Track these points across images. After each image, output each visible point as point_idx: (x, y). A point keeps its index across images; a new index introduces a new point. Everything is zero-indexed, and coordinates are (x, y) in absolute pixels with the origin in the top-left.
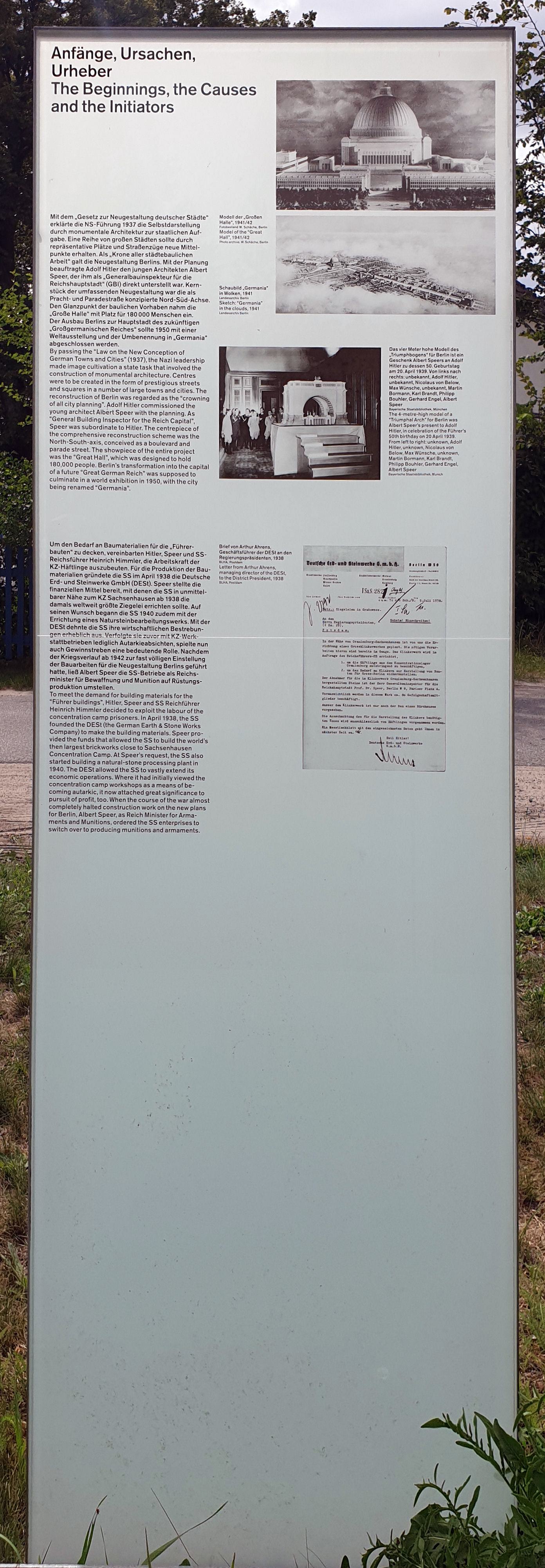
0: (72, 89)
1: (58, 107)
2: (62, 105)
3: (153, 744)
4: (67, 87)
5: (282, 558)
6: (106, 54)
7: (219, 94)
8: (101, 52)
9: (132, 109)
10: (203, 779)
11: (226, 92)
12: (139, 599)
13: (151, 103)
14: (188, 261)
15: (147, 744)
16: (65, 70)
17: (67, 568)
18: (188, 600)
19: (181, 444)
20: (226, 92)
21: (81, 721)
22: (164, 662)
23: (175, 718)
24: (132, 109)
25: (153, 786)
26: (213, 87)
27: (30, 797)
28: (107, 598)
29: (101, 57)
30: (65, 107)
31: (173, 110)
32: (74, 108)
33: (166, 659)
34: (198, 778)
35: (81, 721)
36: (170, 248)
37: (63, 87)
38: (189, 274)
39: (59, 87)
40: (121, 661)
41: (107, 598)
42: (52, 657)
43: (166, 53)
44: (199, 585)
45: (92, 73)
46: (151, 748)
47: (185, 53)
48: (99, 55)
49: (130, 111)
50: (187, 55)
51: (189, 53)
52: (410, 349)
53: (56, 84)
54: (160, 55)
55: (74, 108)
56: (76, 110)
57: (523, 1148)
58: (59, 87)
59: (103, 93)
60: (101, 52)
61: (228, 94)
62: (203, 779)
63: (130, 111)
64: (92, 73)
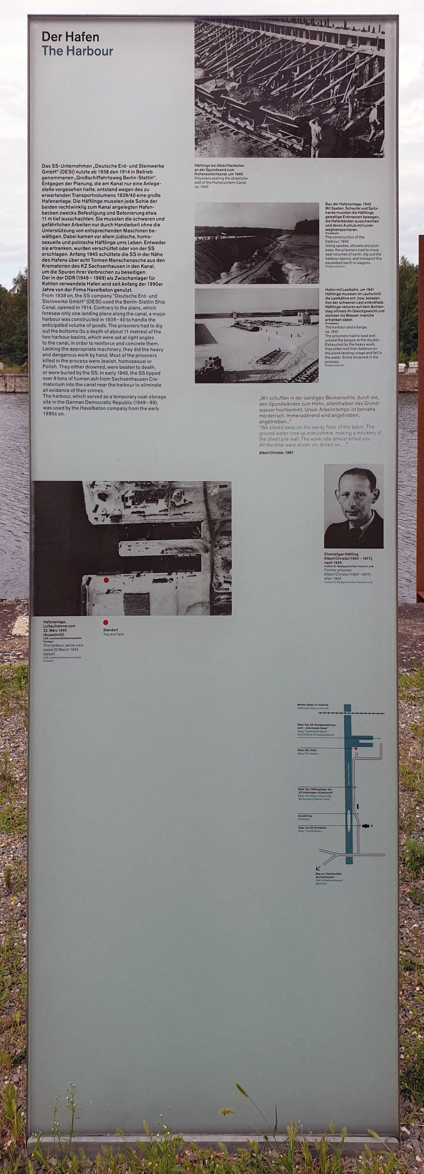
0: (58, 51)
10: (163, 166)
12: (113, 267)
14: (76, 183)
18: (154, 320)
21: (62, 400)
27: (27, 424)
28: (88, 266)
35: (62, 400)
37: (51, 50)
39: (48, 49)
41: (88, 266)
45: (90, 52)
47: (94, 36)
50: (96, 37)
51: (97, 35)
52: (327, 874)
53: (45, 47)
58: (48, 49)
62: (163, 166)
64: (90, 52)
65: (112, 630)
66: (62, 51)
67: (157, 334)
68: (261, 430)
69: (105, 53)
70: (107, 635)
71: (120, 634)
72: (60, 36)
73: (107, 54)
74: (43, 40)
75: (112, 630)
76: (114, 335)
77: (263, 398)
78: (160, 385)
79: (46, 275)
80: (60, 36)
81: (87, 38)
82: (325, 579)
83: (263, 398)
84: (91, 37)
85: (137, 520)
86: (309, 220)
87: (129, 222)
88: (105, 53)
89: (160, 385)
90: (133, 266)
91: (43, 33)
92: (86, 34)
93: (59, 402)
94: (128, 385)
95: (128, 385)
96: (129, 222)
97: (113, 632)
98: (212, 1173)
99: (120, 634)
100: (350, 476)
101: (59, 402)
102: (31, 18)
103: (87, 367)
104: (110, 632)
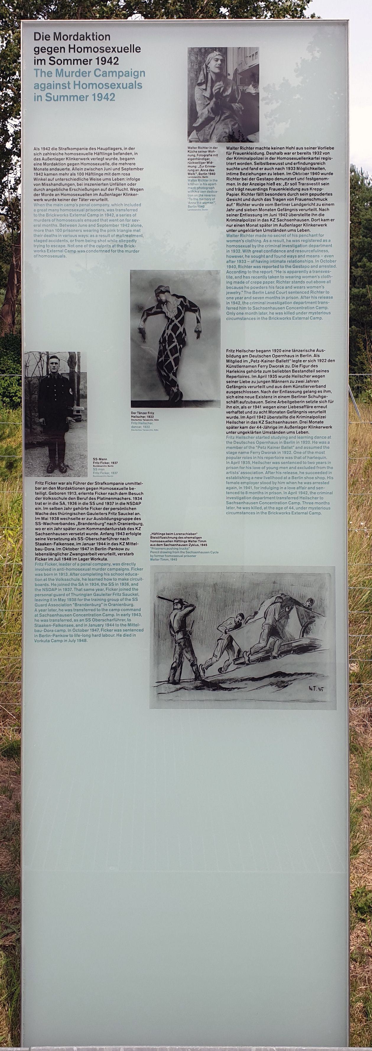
3: (41, 532)
4: (45, 72)
5: (85, 641)
6: (54, 49)
8: (38, 48)
15: (92, 506)
19: (295, 287)
22: (70, 187)
23: (128, 584)
29: (51, 51)
31: (141, 87)
33: (71, 185)
34: (138, 169)
36: (241, 226)
37: (41, 72)
39: (39, 72)
42: (37, 498)
44: (323, 215)
46: (39, 534)
48: (50, 50)
51: (109, 35)
53: (37, 70)
58: (39, 72)
59: (47, 52)
60: (51, 48)
66: (52, 73)
67: (140, 581)
68: (189, 200)
74: (35, 40)
76: (98, 552)
78: (132, 554)
82: (227, 262)
84: (84, 97)
87: (123, 506)
89: (132, 554)
90: (121, 504)
91: (35, 33)
94: (110, 636)
95: (110, 636)
96: (123, 506)
100: (252, 140)
103: (47, 215)
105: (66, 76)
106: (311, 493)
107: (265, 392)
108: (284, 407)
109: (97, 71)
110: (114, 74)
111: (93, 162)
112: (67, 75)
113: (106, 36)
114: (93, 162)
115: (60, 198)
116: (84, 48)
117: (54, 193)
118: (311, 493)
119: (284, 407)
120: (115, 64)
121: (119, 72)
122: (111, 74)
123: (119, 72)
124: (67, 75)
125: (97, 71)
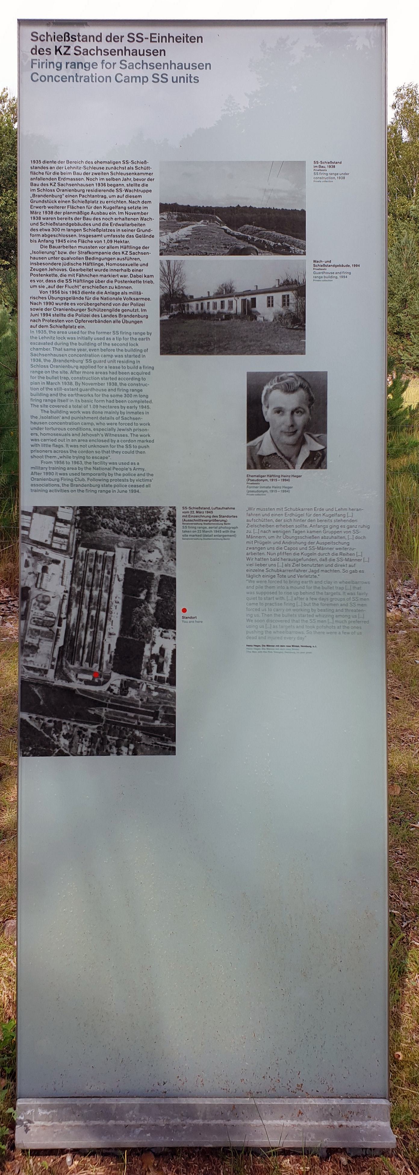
1: (86, 38)
2: (90, 37)
7: (136, 55)
8: (89, 64)
9: (94, 80)
11: (187, 67)
13: (190, 36)
16: (42, 63)
17: (88, 265)
20: (187, 67)
24: (94, 80)
25: (114, 339)
26: (124, 76)
30: (92, 38)
31: (198, 81)
32: (99, 39)
38: (146, 182)
40: (102, 296)
43: (97, 50)
47: (198, 38)
49: (92, 81)
51: (210, 64)
54: (92, 52)
55: (99, 39)
56: (101, 41)
57: (396, 825)
60: (89, 64)
61: (189, 68)
63: (77, 81)
65: (191, 618)
69: (50, 78)
70: (185, 622)
71: (198, 622)
72: (122, 37)
73: (180, 78)
75: (191, 618)
77: (250, 509)
79: (34, 227)
80: (122, 37)
81: (190, 39)
83: (250, 509)
85: (157, 588)
86: (241, 206)
88: (50, 78)
92: (105, 62)
93: (118, 350)
97: (192, 620)
98: (417, 1042)
99: (198, 622)
101: (118, 350)
102: (21, 22)
104: (189, 620)
105: (185, 68)
106: (121, 384)
107: (134, 202)
108: (132, 231)
109: (35, 75)
110: (138, 79)
111: (119, 262)
112: (182, 79)
113: (48, 77)
114: (119, 262)
115: (309, 530)
116: (48, 77)
117: (69, 302)
118: (121, 384)
119: (132, 231)
120: (65, 54)
121: (143, 77)
122: (134, 79)
123: (143, 77)
124: (182, 79)
125: (35, 75)
